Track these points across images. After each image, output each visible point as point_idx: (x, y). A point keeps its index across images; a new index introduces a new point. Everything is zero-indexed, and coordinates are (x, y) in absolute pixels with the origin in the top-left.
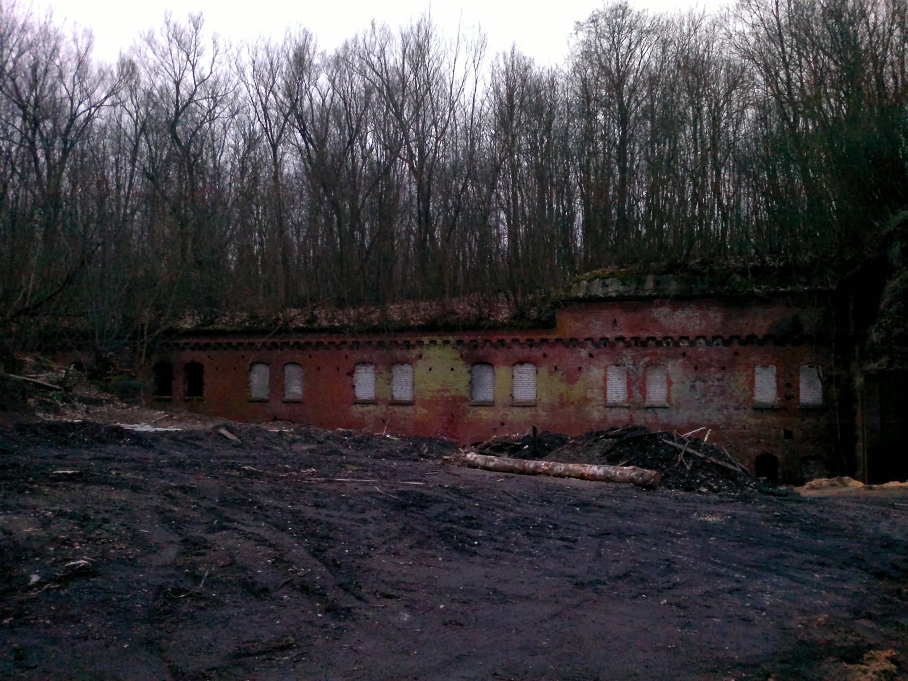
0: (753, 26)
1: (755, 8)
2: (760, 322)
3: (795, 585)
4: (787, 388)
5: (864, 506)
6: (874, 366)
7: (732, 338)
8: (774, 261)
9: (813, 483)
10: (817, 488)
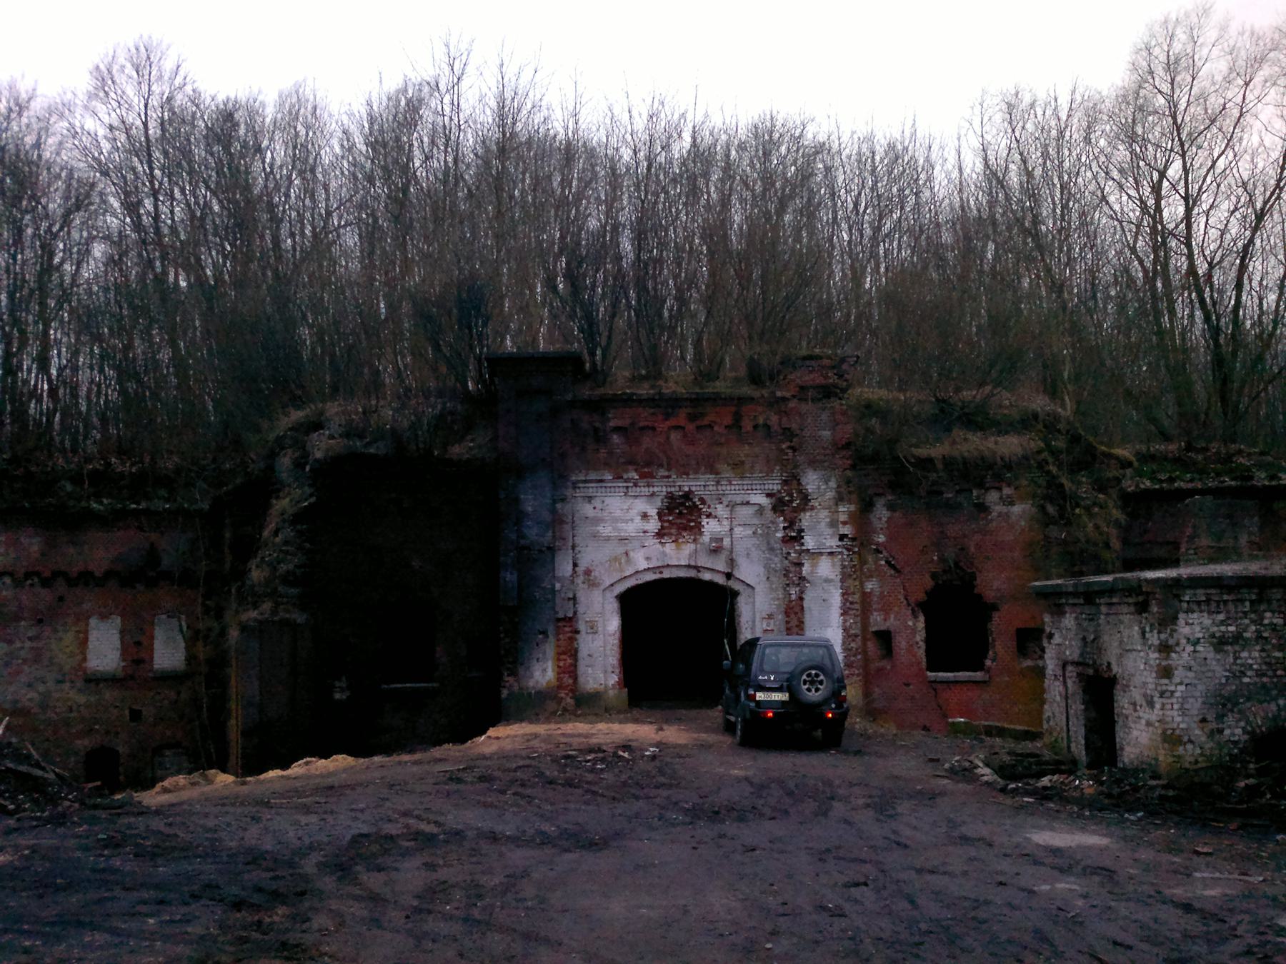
0: (111, 128)
1: (115, 104)
2: (98, 552)
3: (117, 940)
4: (136, 649)
5: (231, 809)
6: (254, 614)
7: (56, 574)
8: (123, 464)
9: (166, 783)
10: (176, 790)
